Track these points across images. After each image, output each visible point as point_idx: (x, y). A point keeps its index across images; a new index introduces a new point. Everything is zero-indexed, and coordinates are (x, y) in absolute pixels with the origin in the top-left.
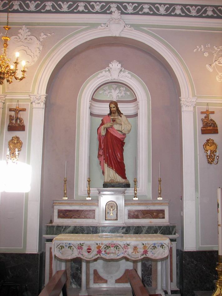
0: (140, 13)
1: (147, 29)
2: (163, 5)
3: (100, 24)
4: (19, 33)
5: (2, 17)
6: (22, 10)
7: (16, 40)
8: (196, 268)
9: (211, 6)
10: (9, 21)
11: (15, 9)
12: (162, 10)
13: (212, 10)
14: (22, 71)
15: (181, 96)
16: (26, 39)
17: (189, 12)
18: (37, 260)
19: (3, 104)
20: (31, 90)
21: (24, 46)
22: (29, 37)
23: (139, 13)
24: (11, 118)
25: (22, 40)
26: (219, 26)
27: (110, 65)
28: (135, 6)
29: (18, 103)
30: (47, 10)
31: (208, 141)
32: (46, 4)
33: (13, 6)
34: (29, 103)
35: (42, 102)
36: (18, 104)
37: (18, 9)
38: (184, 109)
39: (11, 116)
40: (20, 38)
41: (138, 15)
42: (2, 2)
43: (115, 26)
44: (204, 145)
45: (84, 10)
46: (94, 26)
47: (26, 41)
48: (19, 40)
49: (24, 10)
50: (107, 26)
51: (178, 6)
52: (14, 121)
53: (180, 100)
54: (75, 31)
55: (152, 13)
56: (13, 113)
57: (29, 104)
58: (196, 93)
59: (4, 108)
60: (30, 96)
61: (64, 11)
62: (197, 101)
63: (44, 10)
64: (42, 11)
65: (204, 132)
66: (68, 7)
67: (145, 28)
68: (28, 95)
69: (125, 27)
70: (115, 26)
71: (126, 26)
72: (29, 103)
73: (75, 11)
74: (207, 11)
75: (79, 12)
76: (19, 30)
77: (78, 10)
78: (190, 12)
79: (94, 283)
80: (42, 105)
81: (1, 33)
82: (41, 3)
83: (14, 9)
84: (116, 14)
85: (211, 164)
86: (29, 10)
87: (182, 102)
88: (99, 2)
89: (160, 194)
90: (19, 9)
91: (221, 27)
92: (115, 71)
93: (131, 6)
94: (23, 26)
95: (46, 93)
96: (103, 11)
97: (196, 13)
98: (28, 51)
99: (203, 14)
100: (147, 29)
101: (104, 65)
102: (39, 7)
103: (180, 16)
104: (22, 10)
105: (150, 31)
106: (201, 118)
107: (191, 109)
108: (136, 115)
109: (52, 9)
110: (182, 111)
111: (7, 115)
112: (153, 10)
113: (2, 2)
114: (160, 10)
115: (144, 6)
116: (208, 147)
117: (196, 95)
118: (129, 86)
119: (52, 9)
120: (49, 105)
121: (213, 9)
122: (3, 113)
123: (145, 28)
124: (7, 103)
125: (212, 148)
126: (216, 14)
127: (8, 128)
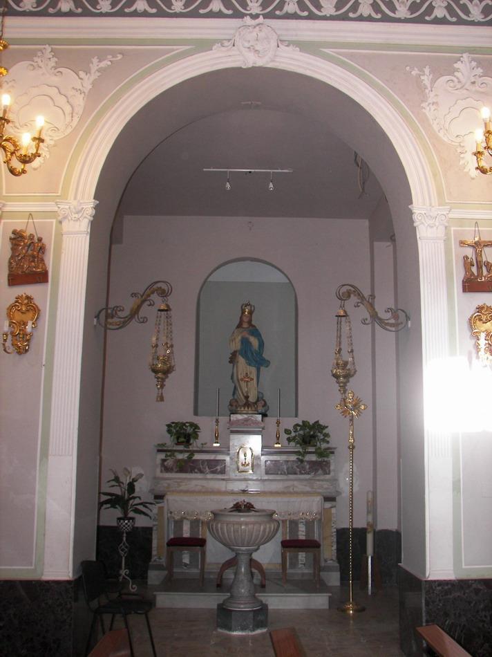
1: (173, 50)
3: (221, 42)
4: (458, 70)
7: (452, 84)
11: (439, 16)
13: (446, 7)
15: (412, 203)
16: (474, 83)
19: (444, 228)
20: (60, 192)
21: (48, 85)
22: (479, 81)
23: (48, 13)
24: (467, 263)
25: (465, 84)
30: (287, 12)
31: (480, 309)
34: (54, 221)
35: (85, 217)
36: (477, 231)
37: (395, 13)
39: (466, 258)
40: (459, 82)
44: (470, 320)
46: (204, 45)
47: (473, 88)
48: (459, 86)
49: (158, 10)
52: (474, 269)
54: (163, 57)
56: (470, 252)
57: (52, 222)
59: (447, 241)
62: (451, 215)
63: (53, 8)
64: (351, 15)
65: (14, 280)
68: (53, 203)
69: (278, 47)
71: (280, 45)
72: (54, 221)
73: (427, 18)
76: (456, 63)
77: (58, 7)
78: (467, 12)
81: (416, 69)
83: (136, 9)
86: (469, 19)
87: (415, 217)
89: (217, 438)
90: (448, 17)
91: (489, 45)
93: (476, 5)
94: (464, 55)
96: (42, 8)
97: (110, 7)
99: (276, 10)
100: (173, 50)
103: (370, 19)
104: (230, 12)
105: (341, 57)
107: (441, 232)
110: (418, 237)
111: (456, 256)
112: (457, 13)
114: (248, 5)
122: (448, 251)
124: (452, 229)
126: (457, 17)
127: (9, 280)
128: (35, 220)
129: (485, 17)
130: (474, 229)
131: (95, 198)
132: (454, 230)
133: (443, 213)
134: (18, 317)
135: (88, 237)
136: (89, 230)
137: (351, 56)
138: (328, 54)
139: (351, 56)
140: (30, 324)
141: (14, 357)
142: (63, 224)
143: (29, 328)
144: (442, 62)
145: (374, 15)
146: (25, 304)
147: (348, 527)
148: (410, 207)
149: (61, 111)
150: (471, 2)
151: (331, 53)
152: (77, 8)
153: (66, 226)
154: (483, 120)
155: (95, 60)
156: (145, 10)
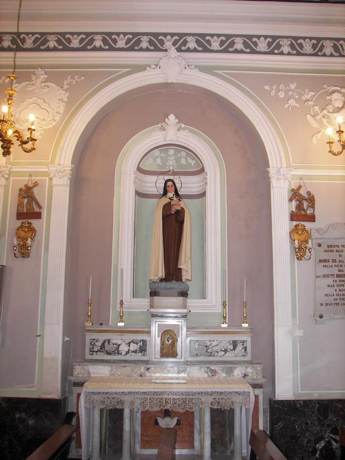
0: (319, 53)
1: (224, 73)
2: (30, 35)
5: (7, 57)
6: (61, 47)
8: (289, 420)
9: (287, 37)
10: (17, 63)
12: (262, 45)
14: (327, 143)
17: (300, 48)
18: (54, 412)
26: (339, 67)
27: (167, 120)
28: (37, 37)
29: (30, 178)
32: (95, 38)
33: (141, 43)
34: (47, 178)
35: (66, 176)
38: (274, 183)
41: (273, 54)
42: (218, 38)
43: (172, 69)
45: (11, 46)
46: (141, 68)
50: (160, 68)
51: (328, 41)
53: (268, 172)
55: (107, 47)
58: (291, 162)
60: (48, 167)
61: (119, 48)
63: (278, 50)
66: (33, 42)
67: (219, 72)
70: (172, 69)
72: (47, 178)
74: (187, 42)
75: (237, 51)
79: (141, 448)
80: (66, 181)
82: (133, 37)
84: (173, 52)
85: (301, 260)
88: (123, 33)
92: (172, 131)
95: (71, 164)
97: (312, 50)
98: (44, 106)
100: (224, 73)
101: (159, 119)
102: (159, 44)
104: (61, 47)
106: (20, 187)
108: (203, 195)
109: (57, 45)
110: (271, 187)
113: (218, 38)
115: (281, 43)
116: (296, 237)
117: (292, 164)
118: (145, 153)
119: (57, 45)
120: (78, 182)
121: (103, 37)
123: (219, 72)
125: (302, 238)
128: (32, 178)
129: (140, 38)
130: (28, 178)
131: (72, 163)
132: (13, 179)
133: (67, 169)
134: (22, 234)
135: (68, 188)
136: (69, 184)
137: (230, 75)
138: (219, 74)
139: (230, 75)
140: (29, 239)
141: (21, 259)
142: (53, 180)
143: (29, 242)
144: (282, 77)
145: (70, 36)
146: (27, 227)
147: (262, 391)
148: (267, 169)
149: (35, 105)
150: (119, 37)
151: (221, 73)
152: (24, 38)
153: (55, 181)
154: (339, 124)
155: (70, 77)
156: (195, 48)
